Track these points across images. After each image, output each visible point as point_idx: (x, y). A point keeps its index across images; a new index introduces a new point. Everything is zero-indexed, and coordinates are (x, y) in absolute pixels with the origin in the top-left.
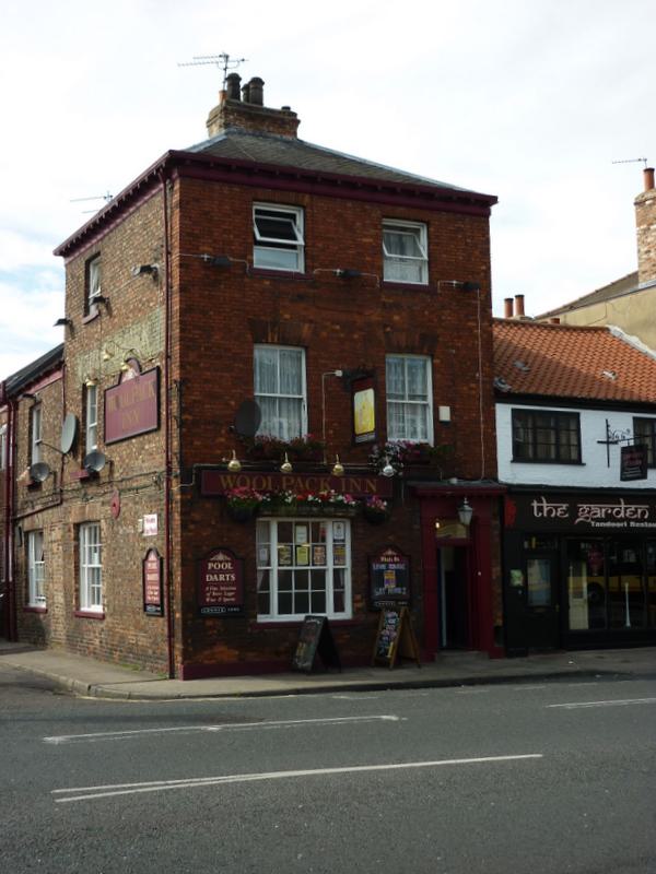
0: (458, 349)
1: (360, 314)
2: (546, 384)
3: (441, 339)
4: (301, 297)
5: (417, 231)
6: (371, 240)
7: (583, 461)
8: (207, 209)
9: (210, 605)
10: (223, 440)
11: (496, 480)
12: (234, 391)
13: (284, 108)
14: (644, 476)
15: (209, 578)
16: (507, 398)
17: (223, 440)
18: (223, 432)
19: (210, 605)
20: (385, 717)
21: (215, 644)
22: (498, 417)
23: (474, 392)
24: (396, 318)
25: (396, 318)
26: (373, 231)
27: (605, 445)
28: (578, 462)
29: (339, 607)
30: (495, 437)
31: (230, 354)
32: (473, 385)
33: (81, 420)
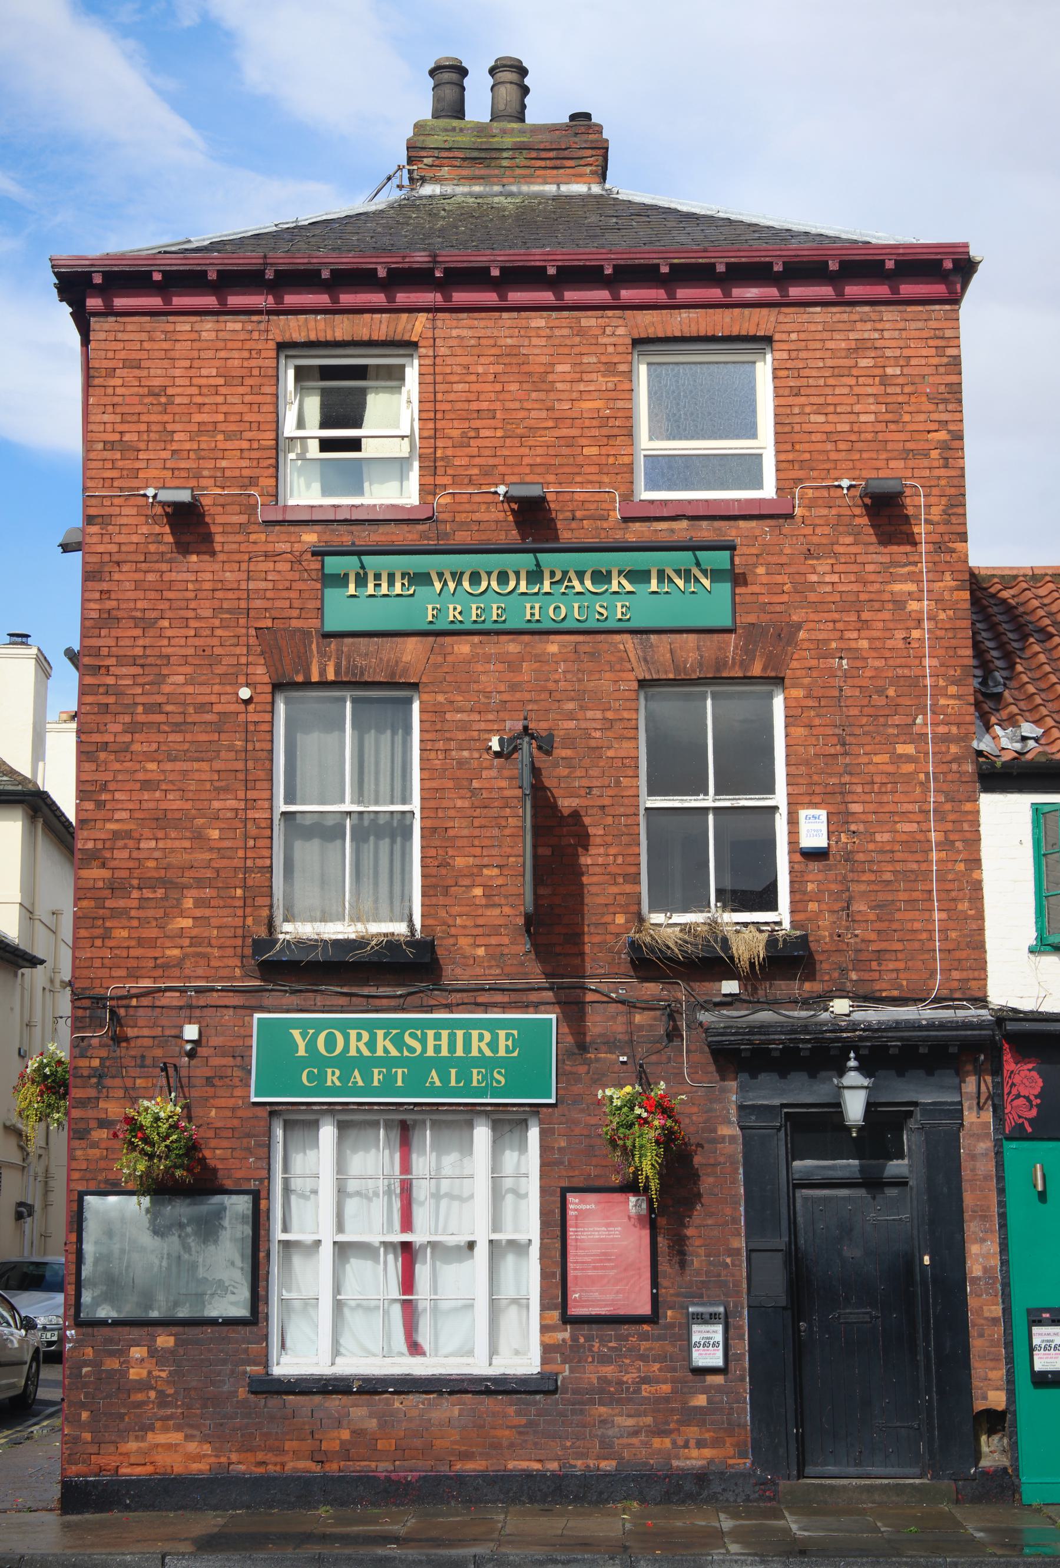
0: (855, 655)
3: (802, 635)
6: (599, 404)
8: (157, 382)
10: (188, 923)
11: (981, 1001)
12: (216, 804)
13: (573, 117)
14: (360, 492)
17: (188, 923)
18: (188, 903)
21: (152, 1428)
23: (909, 768)
26: (603, 382)
31: (209, 717)
32: (910, 749)
33: (210, 1522)
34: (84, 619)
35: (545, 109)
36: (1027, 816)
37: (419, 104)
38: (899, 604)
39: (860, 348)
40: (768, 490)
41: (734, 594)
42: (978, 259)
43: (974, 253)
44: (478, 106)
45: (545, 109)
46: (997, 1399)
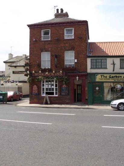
1: (60, 45)
2: (97, 54)
4: (49, 44)
5: (72, 30)
7: (107, 68)
9: (33, 93)
11: (87, 72)
15: (33, 89)
16: (89, 57)
19: (33, 93)
20: (74, 114)
22: (88, 61)
24: (67, 45)
25: (67, 45)
27: (113, 63)
28: (106, 68)
29: (56, 94)
30: (87, 65)
34: (96, 43)
35: (64, 12)
36: (90, 60)
37: (56, 12)
38: (82, 45)
39: (80, 28)
40: (50, 39)
41: (122, 42)
42: (28, 30)
43: (87, 21)
44: (60, 12)
45: (64, 12)
46: (87, 98)
